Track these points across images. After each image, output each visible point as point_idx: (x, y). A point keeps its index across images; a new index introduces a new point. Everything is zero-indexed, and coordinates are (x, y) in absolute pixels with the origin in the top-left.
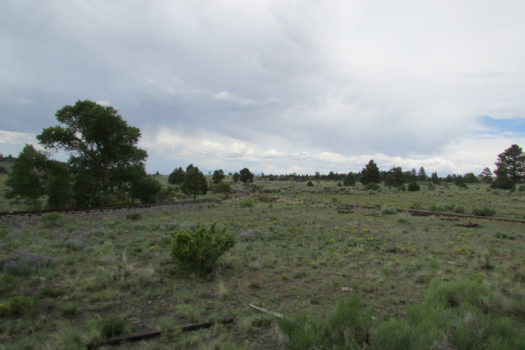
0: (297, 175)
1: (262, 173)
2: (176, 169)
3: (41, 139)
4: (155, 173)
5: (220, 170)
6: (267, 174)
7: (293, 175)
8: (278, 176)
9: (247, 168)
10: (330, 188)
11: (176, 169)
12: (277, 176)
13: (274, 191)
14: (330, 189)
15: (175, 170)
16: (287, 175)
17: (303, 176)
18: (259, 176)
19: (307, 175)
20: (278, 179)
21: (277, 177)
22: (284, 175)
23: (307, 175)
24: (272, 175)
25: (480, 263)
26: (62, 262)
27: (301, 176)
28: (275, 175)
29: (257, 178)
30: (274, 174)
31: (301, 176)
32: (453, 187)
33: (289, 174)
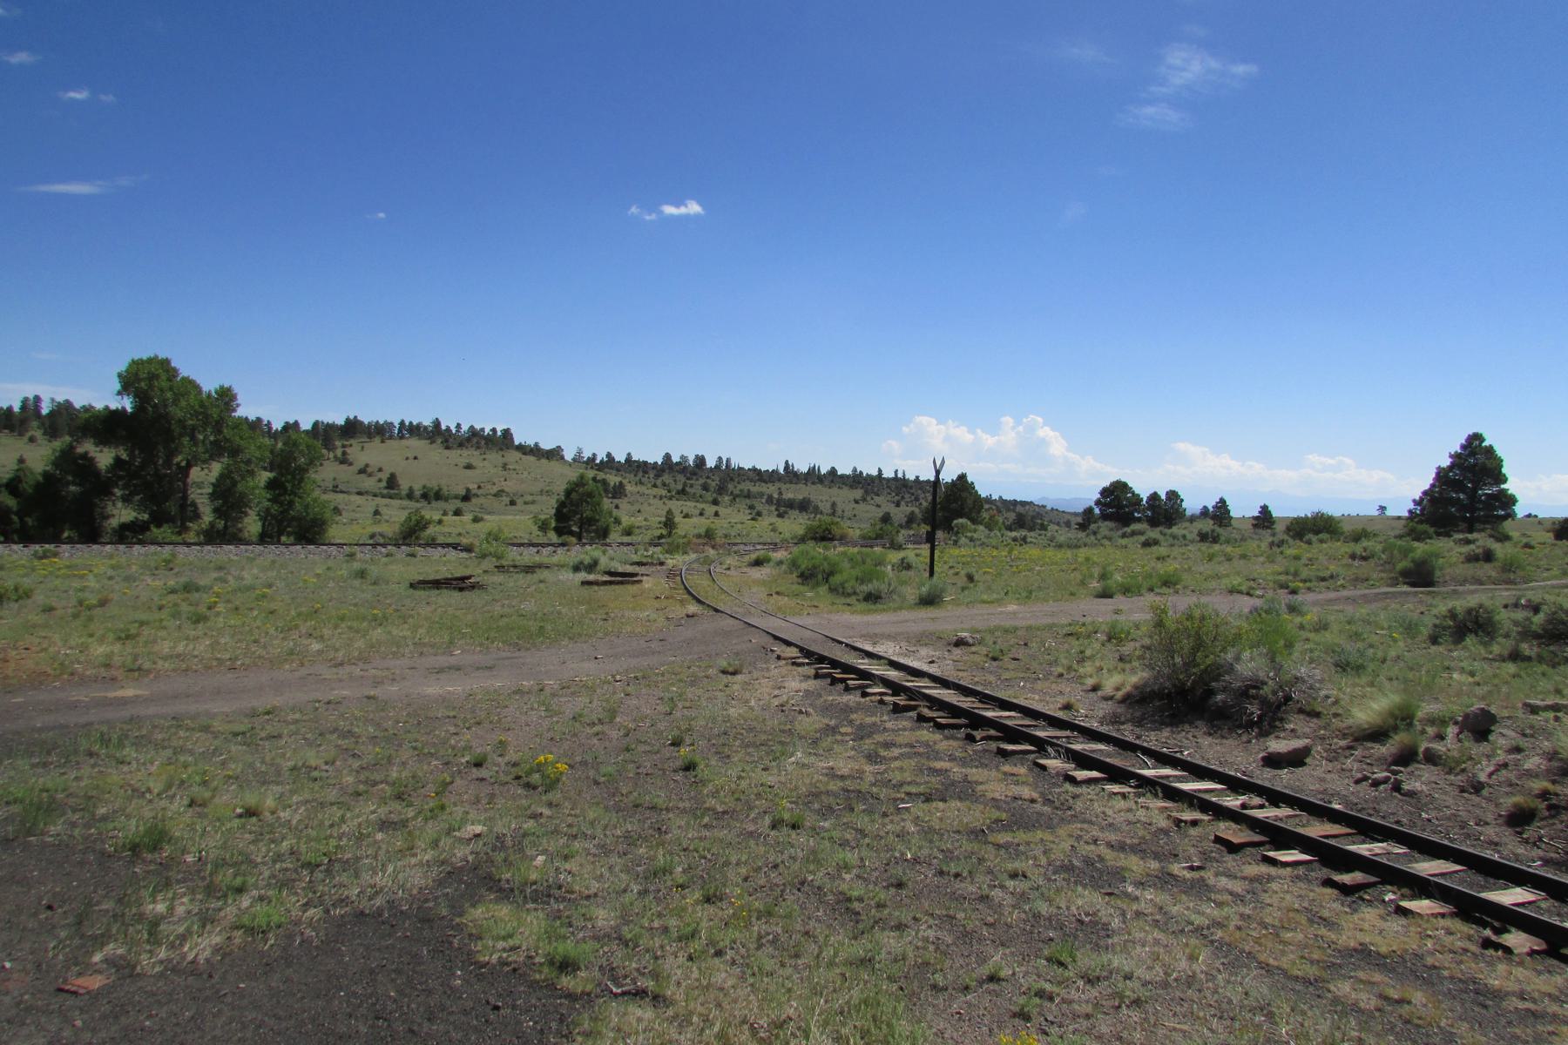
9: (1123, 480)
23: (700, 461)
27: (711, 463)
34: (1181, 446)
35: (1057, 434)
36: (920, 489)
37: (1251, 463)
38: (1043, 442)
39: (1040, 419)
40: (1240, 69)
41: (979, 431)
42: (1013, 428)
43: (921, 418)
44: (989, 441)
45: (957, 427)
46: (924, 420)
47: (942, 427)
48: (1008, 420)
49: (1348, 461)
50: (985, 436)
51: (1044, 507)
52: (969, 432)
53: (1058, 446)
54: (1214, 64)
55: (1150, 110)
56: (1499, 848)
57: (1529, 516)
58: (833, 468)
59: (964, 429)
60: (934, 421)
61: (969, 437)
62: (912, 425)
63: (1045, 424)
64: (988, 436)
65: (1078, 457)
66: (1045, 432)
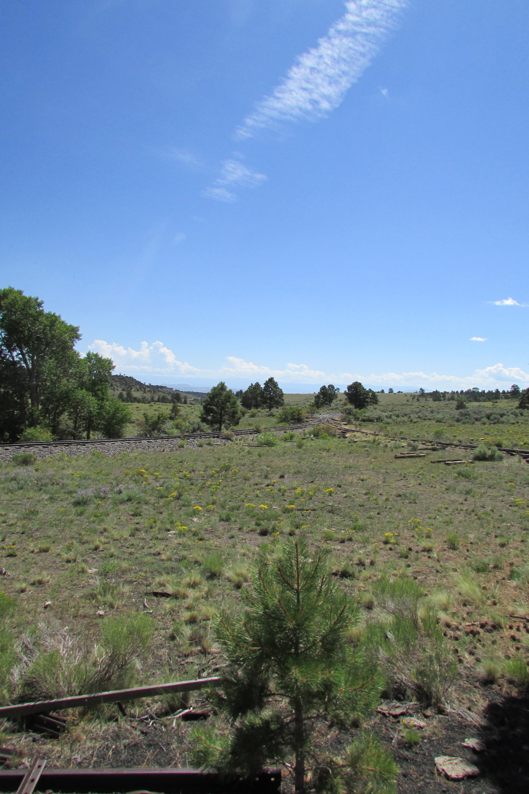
0: (480, 391)
1: (421, 389)
2: (252, 385)
3: (433, 760)
4: (380, 391)
5: (329, 386)
6: (429, 389)
7: (474, 392)
8: (448, 393)
9: (359, 382)
10: (470, 413)
11: (252, 385)
12: (445, 392)
13: (377, 419)
14: (469, 415)
15: (250, 387)
16: (462, 391)
17: (490, 393)
18: (416, 394)
19: (497, 391)
20: (447, 398)
21: (446, 395)
22: (457, 392)
23: (497, 391)
24: (437, 391)
25: (180, 416)
26: (480, 644)
27: (486, 392)
28: (443, 392)
29: (412, 397)
30: (441, 391)
31: (486, 392)
32: (431, 402)
33: (466, 390)
34: (231, 358)
35: (170, 351)
36: (113, 380)
37: (264, 367)
38: (163, 355)
39: (161, 343)
40: (259, 176)
41: (130, 348)
42: (148, 348)
43: (98, 341)
44: (135, 354)
45: (118, 346)
46: (100, 342)
47: (109, 346)
48: (145, 344)
49: (305, 366)
50: (133, 351)
51: (172, 389)
52: (124, 349)
53: (170, 357)
54: (247, 172)
55: (217, 191)
56: (399, 555)
57: (399, 392)
58: (257, 383)
59: (122, 347)
60: (105, 343)
61: (125, 352)
62: (93, 345)
63: (164, 346)
64: (135, 352)
65: (181, 363)
66: (164, 350)
